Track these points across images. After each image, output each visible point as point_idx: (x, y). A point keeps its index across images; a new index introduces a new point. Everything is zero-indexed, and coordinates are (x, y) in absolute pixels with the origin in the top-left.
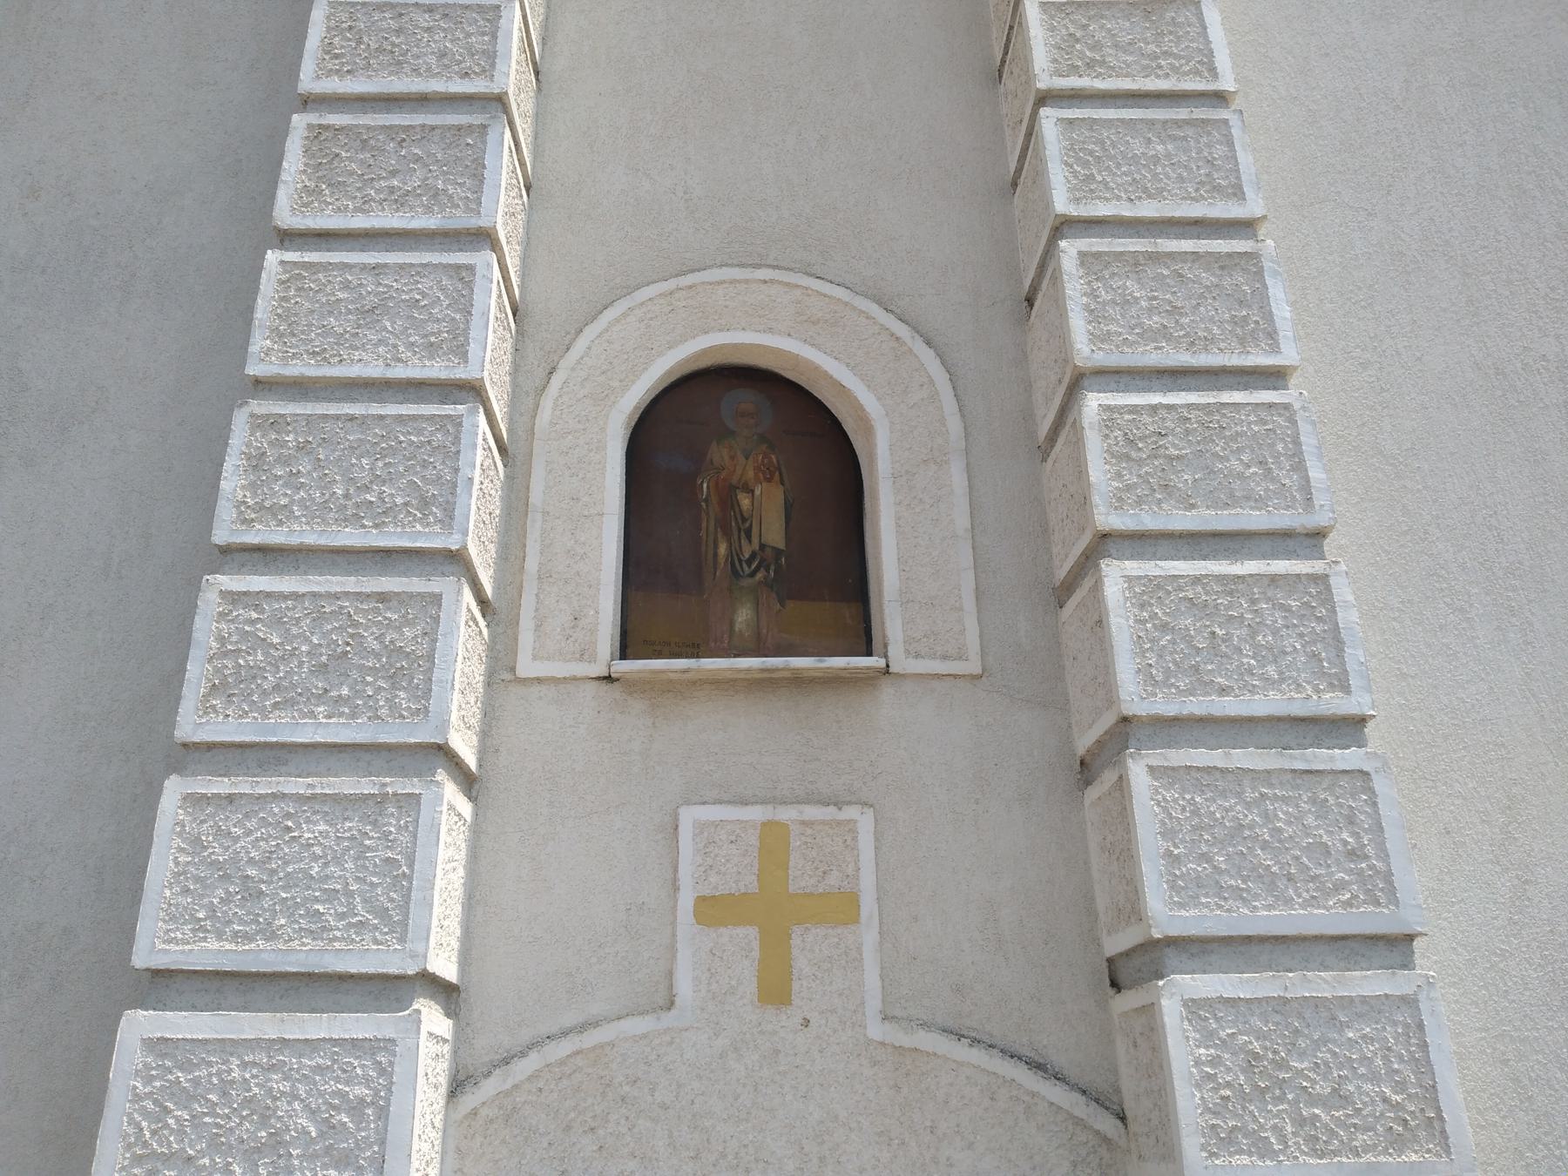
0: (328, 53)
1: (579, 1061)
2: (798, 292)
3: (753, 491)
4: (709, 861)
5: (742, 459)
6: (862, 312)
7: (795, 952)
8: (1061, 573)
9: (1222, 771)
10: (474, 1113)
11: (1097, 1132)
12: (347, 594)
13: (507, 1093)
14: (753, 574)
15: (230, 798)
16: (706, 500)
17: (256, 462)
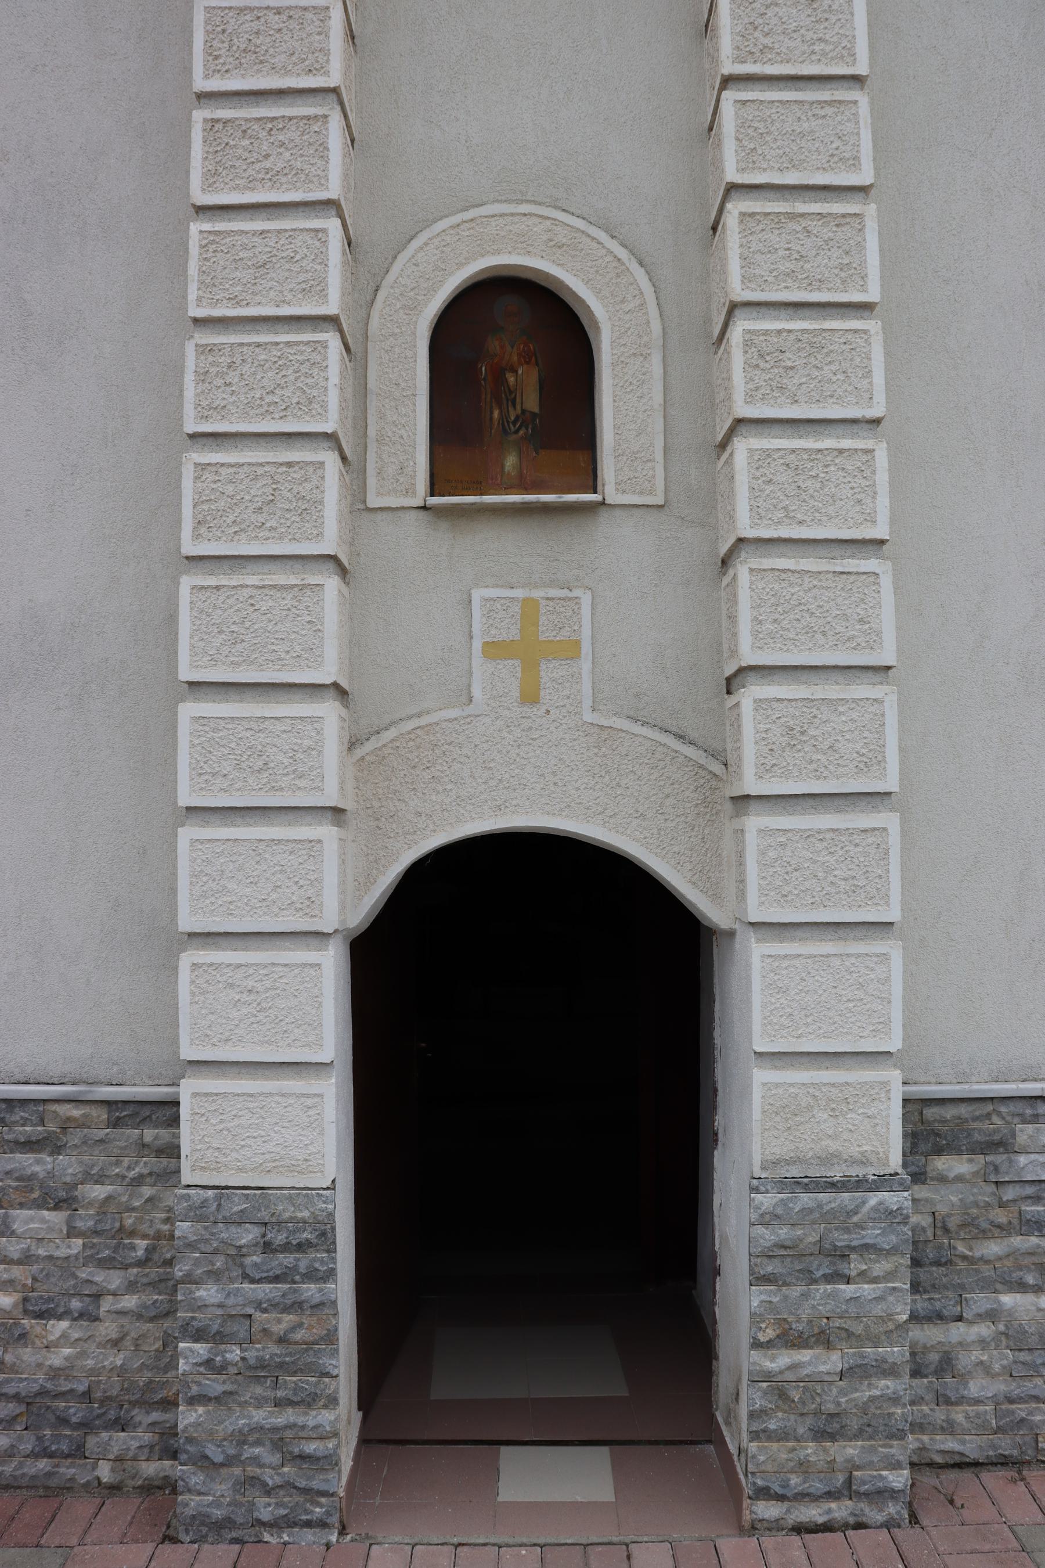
0: (210, 54)
1: (419, 732)
2: (548, 223)
3: (517, 372)
4: (491, 622)
5: (509, 348)
6: (593, 239)
7: (542, 674)
8: (720, 437)
9: (793, 572)
10: (363, 758)
11: (711, 772)
12: (268, 463)
13: (380, 749)
14: (517, 432)
15: (218, 588)
16: (484, 379)
17: (202, 376)
